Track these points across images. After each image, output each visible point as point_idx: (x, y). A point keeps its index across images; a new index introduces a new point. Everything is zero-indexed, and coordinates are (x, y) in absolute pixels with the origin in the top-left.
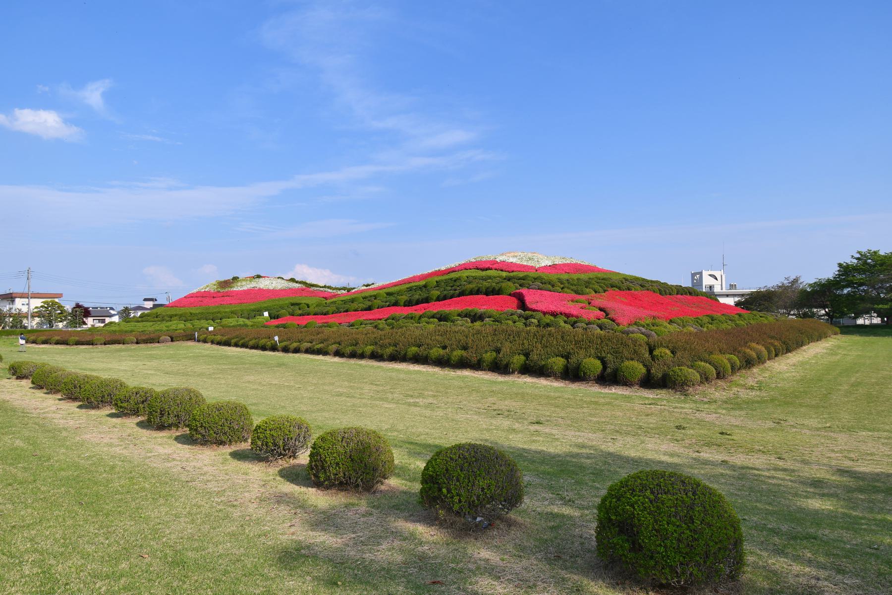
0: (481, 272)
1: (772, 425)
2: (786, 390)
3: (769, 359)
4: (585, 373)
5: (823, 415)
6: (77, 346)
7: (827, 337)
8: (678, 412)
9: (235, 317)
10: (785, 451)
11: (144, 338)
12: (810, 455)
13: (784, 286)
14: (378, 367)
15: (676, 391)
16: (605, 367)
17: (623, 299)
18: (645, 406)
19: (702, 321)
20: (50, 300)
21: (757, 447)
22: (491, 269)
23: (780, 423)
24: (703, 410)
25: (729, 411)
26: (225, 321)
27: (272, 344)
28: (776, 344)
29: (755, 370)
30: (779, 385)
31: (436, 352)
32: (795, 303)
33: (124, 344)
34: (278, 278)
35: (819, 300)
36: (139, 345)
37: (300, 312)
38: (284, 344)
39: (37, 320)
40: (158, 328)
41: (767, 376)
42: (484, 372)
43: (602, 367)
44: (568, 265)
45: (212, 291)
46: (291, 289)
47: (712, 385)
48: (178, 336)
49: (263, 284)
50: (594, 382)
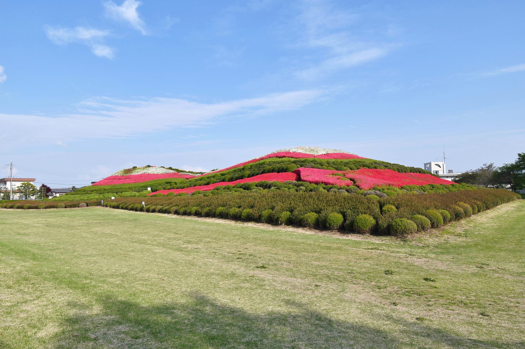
0: (278, 159)
1: (476, 270)
2: (486, 237)
3: (473, 214)
4: (330, 224)
5: (521, 259)
6: (28, 210)
7: (513, 200)
8: (393, 257)
9: (130, 191)
10: (488, 303)
11: (70, 204)
12: (516, 309)
13: (484, 170)
14: (195, 221)
15: (398, 238)
16: (345, 220)
17: (369, 174)
18: (368, 250)
19: (425, 188)
20: (26, 182)
21: (458, 297)
22: (286, 157)
23: (483, 268)
24: (415, 254)
25: (438, 255)
26: (124, 194)
27: (141, 207)
28: (478, 203)
29: (463, 221)
30: (481, 233)
31: (234, 210)
32: (490, 180)
33: (57, 208)
34: (161, 167)
35: (506, 178)
36: (66, 209)
37: (169, 187)
38: (147, 207)
39: (18, 194)
40: (82, 198)
41: (472, 226)
42: (262, 224)
43: (343, 219)
44: (337, 154)
45: (119, 175)
46: (168, 174)
47: (428, 233)
48: (91, 203)
49: (151, 171)
50: (337, 231)
